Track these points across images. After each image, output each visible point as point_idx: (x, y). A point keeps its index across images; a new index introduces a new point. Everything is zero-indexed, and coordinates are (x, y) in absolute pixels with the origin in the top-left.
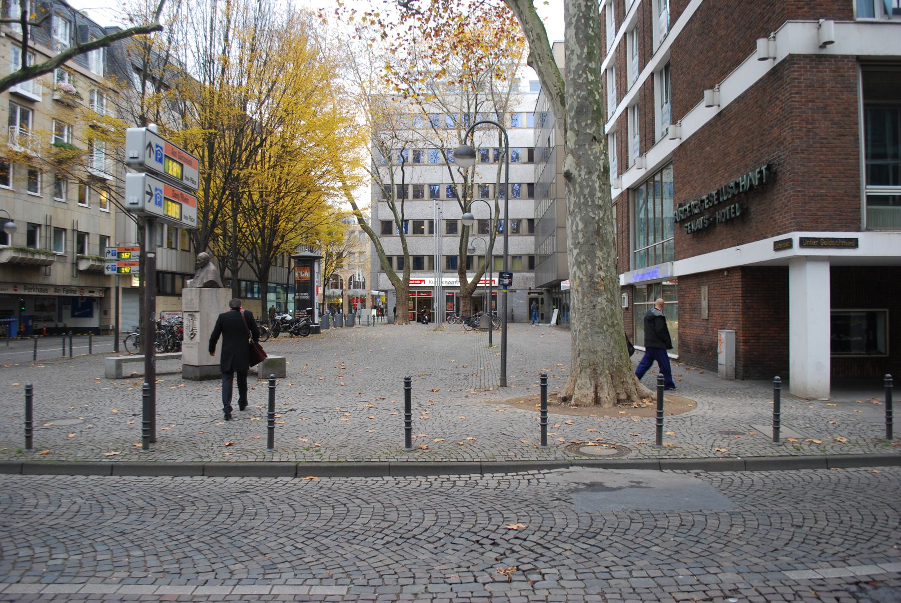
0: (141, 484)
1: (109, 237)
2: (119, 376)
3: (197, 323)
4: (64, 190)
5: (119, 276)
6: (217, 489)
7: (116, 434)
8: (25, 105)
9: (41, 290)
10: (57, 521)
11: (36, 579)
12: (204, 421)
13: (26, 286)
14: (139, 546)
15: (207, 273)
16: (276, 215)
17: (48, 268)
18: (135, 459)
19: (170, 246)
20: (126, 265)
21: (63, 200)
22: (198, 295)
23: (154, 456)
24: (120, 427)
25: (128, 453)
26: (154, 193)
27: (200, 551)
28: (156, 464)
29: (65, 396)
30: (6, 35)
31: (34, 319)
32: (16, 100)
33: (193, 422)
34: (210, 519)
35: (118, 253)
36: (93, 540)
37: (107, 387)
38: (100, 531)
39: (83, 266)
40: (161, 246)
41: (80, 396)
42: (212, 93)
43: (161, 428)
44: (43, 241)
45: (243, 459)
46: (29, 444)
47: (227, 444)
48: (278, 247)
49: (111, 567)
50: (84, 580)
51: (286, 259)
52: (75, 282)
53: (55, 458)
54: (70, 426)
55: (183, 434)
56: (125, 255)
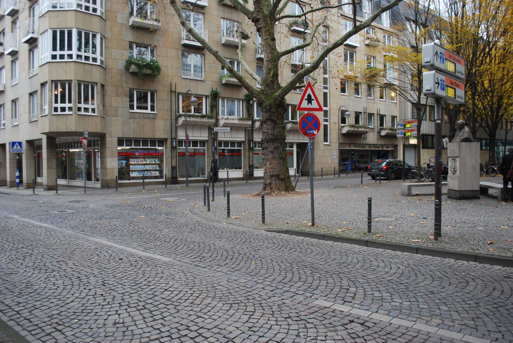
0: (436, 262)
1: (396, 117)
2: (410, 195)
3: (458, 164)
4: (372, 93)
5: (405, 137)
6: (487, 272)
7: (416, 229)
8: (351, 50)
9: (362, 147)
10: (391, 278)
11: (387, 312)
12: (469, 226)
13: (355, 145)
14: (444, 303)
15: (464, 133)
16: (501, 95)
17: (365, 135)
18: (430, 245)
19: (430, 120)
20: (409, 131)
21: (372, 98)
22: (458, 146)
23: (442, 245)
24: (417, 225)
25: (426, 241)
26: (440, 83)
27: (487, 315)
28: (444, 250)
29: (382, 204)
30: (341, 15)
31: (359, 162)
32: (347, 48)
33: (462, 226)
34: (489, 293)
35: (404, 125)
36: (415, 293)
37: (404, 200)
38: (418, 289)
39: (383, 133)
40: (426, 120)
41: (391, 205)
42: (451, 24)
43: (444, 229)
44: (363, 121)
45: (503, 254)
46: (369, 231)
47: (489, 242)
48: (502, 115)
49: (429, 314)
50: (415, 319)
51: (504, 123)
52: (379, 142)
53: (384, 239)
54: (389, 221)
55: (457, 233)
56: (408, 126)
